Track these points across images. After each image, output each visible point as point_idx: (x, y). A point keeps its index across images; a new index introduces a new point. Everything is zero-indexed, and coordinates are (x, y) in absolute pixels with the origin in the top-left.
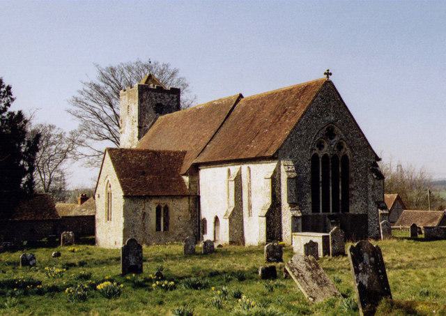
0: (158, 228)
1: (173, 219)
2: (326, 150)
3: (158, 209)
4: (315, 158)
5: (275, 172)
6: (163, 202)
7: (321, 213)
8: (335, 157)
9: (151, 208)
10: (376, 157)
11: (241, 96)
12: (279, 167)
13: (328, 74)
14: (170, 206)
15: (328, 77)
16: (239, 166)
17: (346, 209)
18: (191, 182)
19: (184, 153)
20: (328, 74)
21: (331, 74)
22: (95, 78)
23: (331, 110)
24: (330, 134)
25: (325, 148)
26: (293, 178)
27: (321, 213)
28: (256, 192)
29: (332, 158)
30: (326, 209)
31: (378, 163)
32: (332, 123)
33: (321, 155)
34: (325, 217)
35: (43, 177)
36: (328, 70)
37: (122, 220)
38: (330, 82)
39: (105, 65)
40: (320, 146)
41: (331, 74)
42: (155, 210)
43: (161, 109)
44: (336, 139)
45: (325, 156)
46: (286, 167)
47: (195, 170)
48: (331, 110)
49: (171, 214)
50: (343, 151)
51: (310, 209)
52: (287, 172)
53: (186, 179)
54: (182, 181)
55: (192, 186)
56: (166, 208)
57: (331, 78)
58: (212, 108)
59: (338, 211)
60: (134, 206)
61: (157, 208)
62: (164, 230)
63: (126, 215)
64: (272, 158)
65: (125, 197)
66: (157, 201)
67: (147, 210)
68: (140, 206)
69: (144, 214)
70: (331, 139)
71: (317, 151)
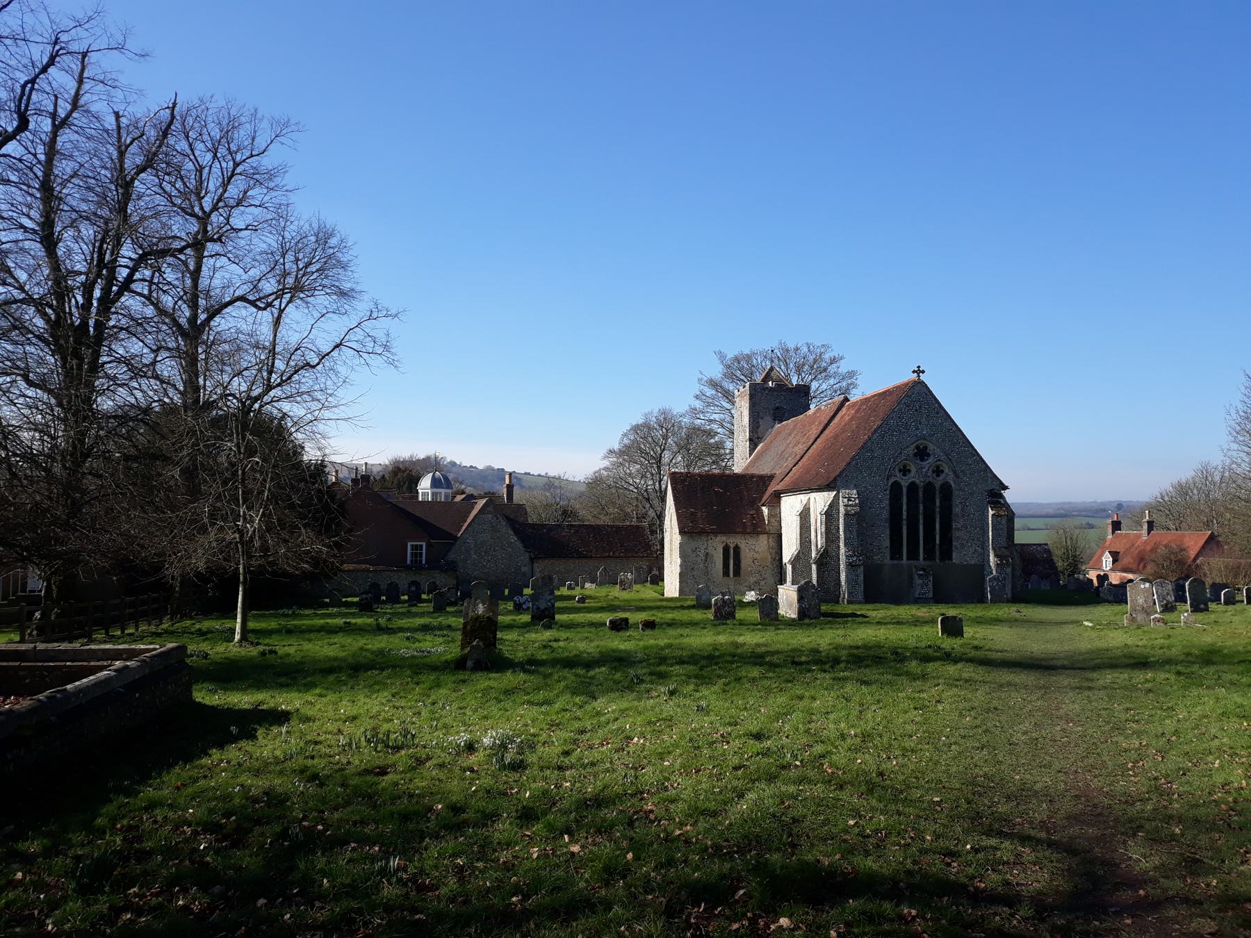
0: (726, 573)
1: (746, 562)
2: (913, 476)
3: (726, 550)
4: (896, 487)
6: (732, 541)
8: (929, 487)
9: (716, 546)
10: (1001, 483)
13: (919, 371)
14: (742, 546)
15: (919, 376)
16: (807, 497)
17: (947, 554)
18: (770, 515)
19: (771, 477)
20: (919, 371)
21: (923, 372)
22: (716, 371)
24: (922, 453)
25: (912, 474)
26: (853, 515)
29: (925, 487)
30: (913, 555)
31: (1006, 494)
32: (925, 439)
33: (937, 486)
35: (72, 127)
36: (919, 367)
37: (679, 561)
38: (922, 384)
42: (721, 551)
44: (931, 460)
45: (913, 487)
46: (846, 500)
47: (777, 497)
48: (923, 420)
49: (743, 555)
50: (942, 476)
51: (888, 558)
52: (845, 506)
53: (765, 510)
54: (761, 513)
55: (773, 520)
56: (737, 549)
57: (923, 377)
59: (901, 558)
61: (723, 548)
62: (734, 575)
63: (683, 555)
65: (682, 532)
67: (710, 550)
68: (702, 544)
70: (922, 460)
71: (898, 477)
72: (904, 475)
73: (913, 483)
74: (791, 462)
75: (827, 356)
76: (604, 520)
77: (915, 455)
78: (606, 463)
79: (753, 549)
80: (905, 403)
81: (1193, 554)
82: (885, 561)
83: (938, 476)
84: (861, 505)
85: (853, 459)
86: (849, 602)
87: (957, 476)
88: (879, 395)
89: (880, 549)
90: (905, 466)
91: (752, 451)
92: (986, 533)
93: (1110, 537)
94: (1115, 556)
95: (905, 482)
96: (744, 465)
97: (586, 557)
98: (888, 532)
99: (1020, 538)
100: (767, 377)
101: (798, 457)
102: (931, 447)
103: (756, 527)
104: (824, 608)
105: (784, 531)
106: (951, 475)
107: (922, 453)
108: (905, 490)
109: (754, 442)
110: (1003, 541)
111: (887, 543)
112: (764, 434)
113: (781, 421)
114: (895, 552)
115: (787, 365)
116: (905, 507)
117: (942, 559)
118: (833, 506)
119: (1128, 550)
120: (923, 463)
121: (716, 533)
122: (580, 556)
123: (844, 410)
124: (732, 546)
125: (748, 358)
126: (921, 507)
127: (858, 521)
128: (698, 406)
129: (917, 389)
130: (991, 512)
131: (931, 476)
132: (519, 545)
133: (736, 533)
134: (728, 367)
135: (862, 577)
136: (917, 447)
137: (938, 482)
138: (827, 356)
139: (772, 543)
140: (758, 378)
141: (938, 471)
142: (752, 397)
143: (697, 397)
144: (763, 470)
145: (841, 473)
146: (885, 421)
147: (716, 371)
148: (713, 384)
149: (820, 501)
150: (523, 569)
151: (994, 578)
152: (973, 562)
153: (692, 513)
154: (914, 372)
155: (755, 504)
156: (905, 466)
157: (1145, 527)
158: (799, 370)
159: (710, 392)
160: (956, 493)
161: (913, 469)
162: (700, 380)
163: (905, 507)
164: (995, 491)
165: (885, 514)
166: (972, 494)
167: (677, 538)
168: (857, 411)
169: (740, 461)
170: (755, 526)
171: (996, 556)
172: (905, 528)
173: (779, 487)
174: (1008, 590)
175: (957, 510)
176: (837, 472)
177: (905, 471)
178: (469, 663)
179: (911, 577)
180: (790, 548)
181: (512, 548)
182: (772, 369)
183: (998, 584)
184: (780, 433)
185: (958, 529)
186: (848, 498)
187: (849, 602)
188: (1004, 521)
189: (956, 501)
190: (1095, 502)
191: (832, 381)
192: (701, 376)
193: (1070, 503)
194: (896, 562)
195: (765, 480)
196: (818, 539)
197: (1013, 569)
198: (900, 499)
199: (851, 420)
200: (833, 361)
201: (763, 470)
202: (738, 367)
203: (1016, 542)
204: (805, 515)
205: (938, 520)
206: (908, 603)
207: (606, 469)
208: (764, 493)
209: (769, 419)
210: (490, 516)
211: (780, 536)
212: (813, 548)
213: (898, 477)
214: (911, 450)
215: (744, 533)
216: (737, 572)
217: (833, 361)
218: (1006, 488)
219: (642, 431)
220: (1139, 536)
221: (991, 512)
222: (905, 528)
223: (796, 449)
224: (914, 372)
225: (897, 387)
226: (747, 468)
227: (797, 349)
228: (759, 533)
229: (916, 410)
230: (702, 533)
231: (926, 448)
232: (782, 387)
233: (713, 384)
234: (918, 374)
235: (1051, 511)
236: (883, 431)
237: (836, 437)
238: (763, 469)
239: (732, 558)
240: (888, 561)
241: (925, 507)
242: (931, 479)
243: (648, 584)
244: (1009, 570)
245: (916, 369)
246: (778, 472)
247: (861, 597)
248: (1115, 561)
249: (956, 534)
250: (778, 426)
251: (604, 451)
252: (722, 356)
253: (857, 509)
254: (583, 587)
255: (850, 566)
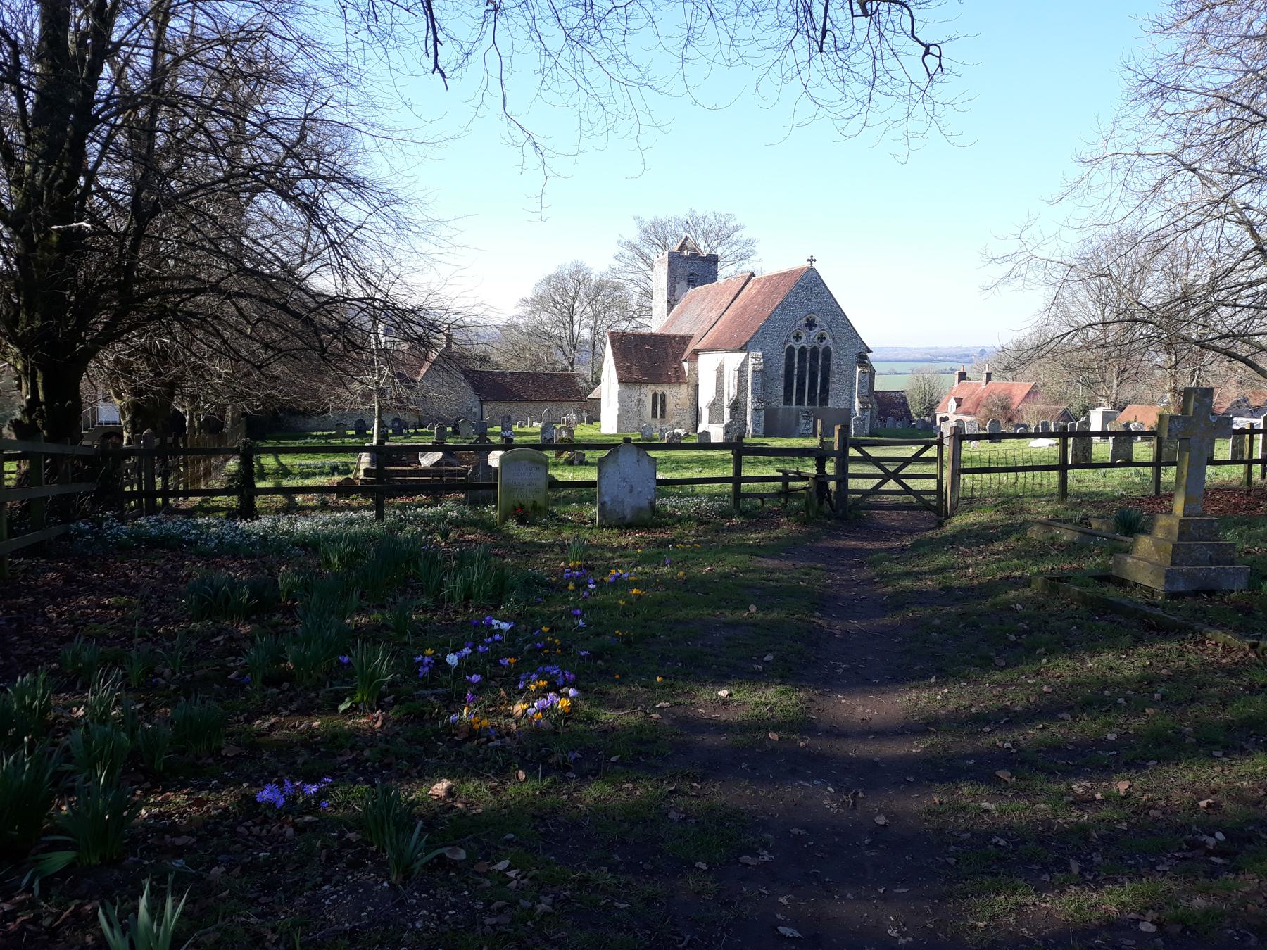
0: (654, 415)
2: (803, 342)
3: (655, 396)
4: (790, 351)
5: (742, 364)
6: (660, 389)
7: (794, 406)
8: (814, 351)
9: (647, 393)
11: (753, 275)
12: (747, 358)
14: (667, 394)
17: (824, 401)
19: (690, 337)
20: (812, 260)
22: (634, 235)
24: (811, 324)
25: (803, 340)
27: (794, 406)
30: (800, 401)
31: (869, 355)
33: (821, 350)
34: (797, 411)
37: (617, 405)
38: (813, 269)
39: (648, 218)
43: (693, 281)
44: (817, 329)
47: (696, 353)
48: (813, 299)
49: (667, 401)
50: (825, 342)
51: (782, 400)
53: (686, 365)
56: (663, 395)
58: (770, 278)
60: (629, 392)
62: (661, 416)
63: (621, 401)
64: (741, 350)
65: (621, 382)
67: (642, 397)
68: (636, 392)
70: (811, 329)
71: (792, 342)
73: (803, 347)
74: (706, 326)
75: (730, 225)
76: (521, 367)
77: (806, 325)
78: (519, 311)
79: (676, 396)
81: (1017, 400)
84: (765, 363)
85: (760, 328)
86: (753, 437)
87: (835, 342)
88: (780, 275)
90: (798, 334)
91: (669, 311)
92: (853, 385)
93: (956, 385)
94: (959, 402)
95: (797, 347)
96: (662, 324)
97: (526, 400)
98: (783, 384)
99: (882, 384)
100: (683, 246)
101: (713, 322)
102: (817, 319)
103: (679, 379)
104: (819, 421)
105: (700, 383)
106: (831, 342)
107: (811, 324)
108: (797, 352)
109: (671, 304)
110: (866, 391)
111: (782, 392)
112: (679, 297)
113: (694, 286)
114: (788, 400)
115: (696, 232)
116: (796, 366)
117: (821, 404)
118: (744, 364)
119: (969, 397)
121: (647, 383)
122: (522, 400)
123: (751, 283)
125: (662, 224)
126: (808, 365)
127: (763, 376)
128: (617, 266)
129: (810, 273)
130: (858, 370)
131: (817, 343)
133: (663, 383)
134: (645, 231)
135: (763, 418)
136: (808, 320)
138: (730, 225)
139: (691, 392)
140: (675, 248)
141: (822, 338)
142: (670, 264)
143: (616, 258)
144: (681, 330)
145: (751, 339)
146: (785, 299)
147: (634, 235)
148: (632, 247)
149: (733, 361)
150: (474, 410)
151: (858, 419)
153: (628, 367)
155: (677, 358)
156: (798, 334)
157: (985, 378)
158: (706, 235)
159: (627, 253)
160: (833, 355)
161: (804, 337)
162: (619, 242)
163: (796, 366)
164: (862, 356)
165: (782, 371)
166: (845, 356)
167: (616, 387)
168: (762, 287)
169: (657, 322)
170: (678, 378)
171: (860, 402)
173: (697, 347)
174: (867, 428)
175: (834, 367)
176: (748, 339)
177: (798, 338)
178: (576, 462)
179: (798, 420)
180: (706, 396)
182: (687, 239)
184: (694, 297)
186: (754, 359)
187: (753, 437)
188: (867, 377)
189: (834, 360)
190: (960, 347)
191: (734, 248)
192: (620, 238)
193: (937, 348)
195: (685, 340)
196: (731, 391)
197: (872, 413)
198: (793, 359)
199: (758, 293)
200: (736, 229)
201: (681, 330)
202: (655, 233)
204: (720, 371)
206: (795, 437)
207: (519, 317)
208: (684, 350)
209: (684, 283)
211: (697, 386)
212: (726, 396)
213: (792, 342)
214: (803, 322)
215: (670, 383)
217: (736, 229)
218: (870, 351)
219: (556, 283)
220: (980, 385)
221: (858, 370)
223: (710, 314)
225: (794, 271)
226: (665, 327)
227: (705, 217)
228: (680, 384)
230: (637, 382)
231: (814, 320)
232: (695, 256)
233: (632, 247)
235: (918, 356)
236: (783, 307)
237: (745, 307)
238: (680, 329)
239: (659, 403)
240: (781, 406)
241: (811, 365)
242: (816, 344)
243: (585, 424)
244: (868, 413)
246: (696, 333)
247: (761, 433)
248: (958, 406)
249: (832, 386)
250: (691, 290)
251: (517, 300)
252: (640, 222)
253: (762, 367)
254: (531, 426)
255: (756, 410)
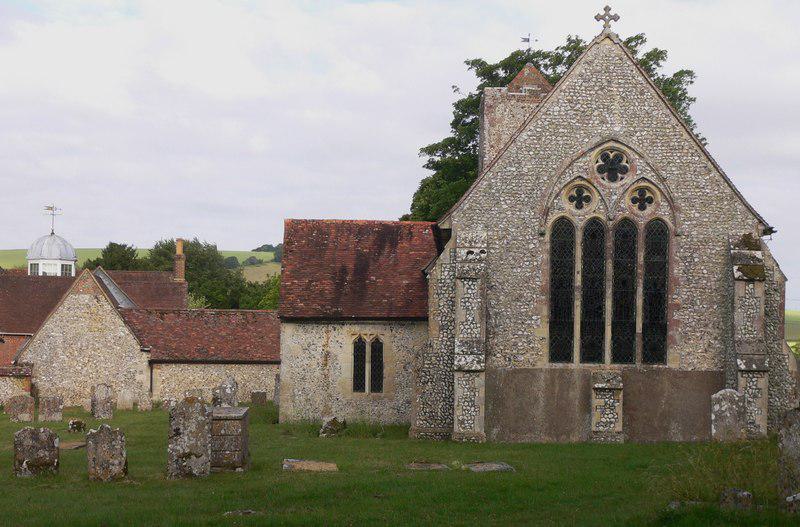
0: (358, 386)
3: (359, 346)
4: (563, 228)
8: (626, 229)
14: (386, 339)
17: (656, 351)
21: (616, 18)
23: (616, 106)
24: (613, 167)
28: (146, 278)
30: (592, 353)
33: (642, 223)
40: (580, 199)
41: (616, 18)
42: (349, 349)
44: (628, 179)
45: (594, 229)
50: (650, 209)
56: (377, 347)
59: (568, 358)
61: (355, 343)
66: (356, 329)
67: (333, 348)
69: (327, 355)
70: (613, 178)
71: (568, 209)
72: (579, 206)
73: (594, 221)
77: (600, 170)
80: (581, 75)
82: (539, 365)
83: (642, 208)
89: (529, 343)
114: (560, 350)
120: (613, 185)
124: (368, 340)
131: (628, 208)
132: (132, 341)
137: (643, 218)
150: (139, 377)
152: (704, 367)
154: (598, 18)
165: (542, 279)
172: (578, 303)
175: (677, 271)
181: (121, 345)
183: (731, 409)
185: (678, 307)
194: (560, 365)
203: (59, 274)
205: (640, 290)
210: (87, 297)
214: (593, 160)
216: (377, 386)
218: (769, 231)
222: (578, 303)
224: (598, 18)
229: (602, 89)
234: (607, 22)
240: (544, 363)
241: (616, 266)
245: (602, 13)
